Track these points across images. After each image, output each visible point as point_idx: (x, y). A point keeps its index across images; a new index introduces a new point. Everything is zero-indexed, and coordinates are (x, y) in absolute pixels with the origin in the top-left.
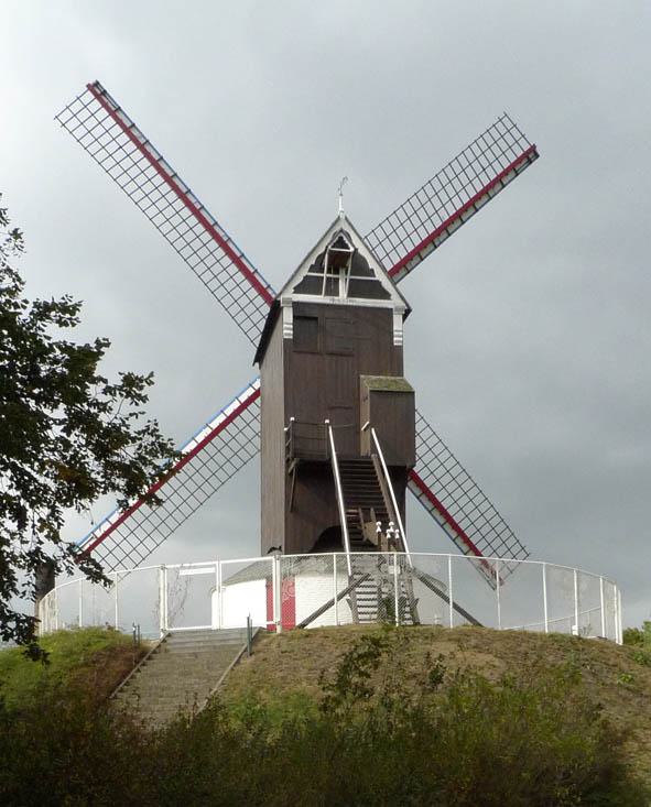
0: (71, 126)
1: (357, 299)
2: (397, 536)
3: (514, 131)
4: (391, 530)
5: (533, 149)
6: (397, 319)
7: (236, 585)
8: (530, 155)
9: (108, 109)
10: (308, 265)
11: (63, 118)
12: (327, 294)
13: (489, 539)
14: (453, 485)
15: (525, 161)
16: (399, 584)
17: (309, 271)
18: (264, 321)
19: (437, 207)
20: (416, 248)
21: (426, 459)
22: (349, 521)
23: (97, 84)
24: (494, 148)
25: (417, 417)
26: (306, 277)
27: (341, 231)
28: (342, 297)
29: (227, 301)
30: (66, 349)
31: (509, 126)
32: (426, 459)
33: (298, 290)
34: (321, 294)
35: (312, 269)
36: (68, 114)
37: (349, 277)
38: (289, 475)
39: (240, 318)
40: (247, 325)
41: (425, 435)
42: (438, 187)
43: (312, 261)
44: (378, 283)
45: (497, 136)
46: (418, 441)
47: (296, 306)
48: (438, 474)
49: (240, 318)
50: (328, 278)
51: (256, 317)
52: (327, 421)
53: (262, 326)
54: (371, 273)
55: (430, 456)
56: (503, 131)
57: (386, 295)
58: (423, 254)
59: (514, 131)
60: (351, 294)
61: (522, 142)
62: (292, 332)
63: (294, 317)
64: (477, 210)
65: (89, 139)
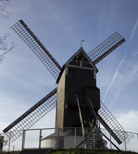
0: (15, 29)
3: (119, 35)
5: (124, 39)
6: (95, 72)
7: (49, 135)
9: (27, 29)
11: (13, 27)
13: (110, 121)
15: (122, 41)
16: (93, 141)
17: (73, 60)
18: (59, 74)
19: (93, 55)
20: (103, 54)
23: (22, 20)
24: (101, 49)
26: (71, 61)
27: (82, 51)
28: (81, 67)
33: (69, 64)
35: (73, 59)
36: (14, 27)
37: (83, 62)
38: (65, 109)
40: (55, 75)
43: (74, 57)
44: (90, 64)
45: (105, 44)
47: (69, 67)
50: (76, 62)
51: (57, 73)
53: (58, 75)
54: (89, 62)
56: (103, 45)
57: (92, 67)
58: (105, 55)
59: (119, 35)
60: (83, 66)
61: (121, 37)
63: (68, 70)
64: (108, 54)
65: (19, 32)
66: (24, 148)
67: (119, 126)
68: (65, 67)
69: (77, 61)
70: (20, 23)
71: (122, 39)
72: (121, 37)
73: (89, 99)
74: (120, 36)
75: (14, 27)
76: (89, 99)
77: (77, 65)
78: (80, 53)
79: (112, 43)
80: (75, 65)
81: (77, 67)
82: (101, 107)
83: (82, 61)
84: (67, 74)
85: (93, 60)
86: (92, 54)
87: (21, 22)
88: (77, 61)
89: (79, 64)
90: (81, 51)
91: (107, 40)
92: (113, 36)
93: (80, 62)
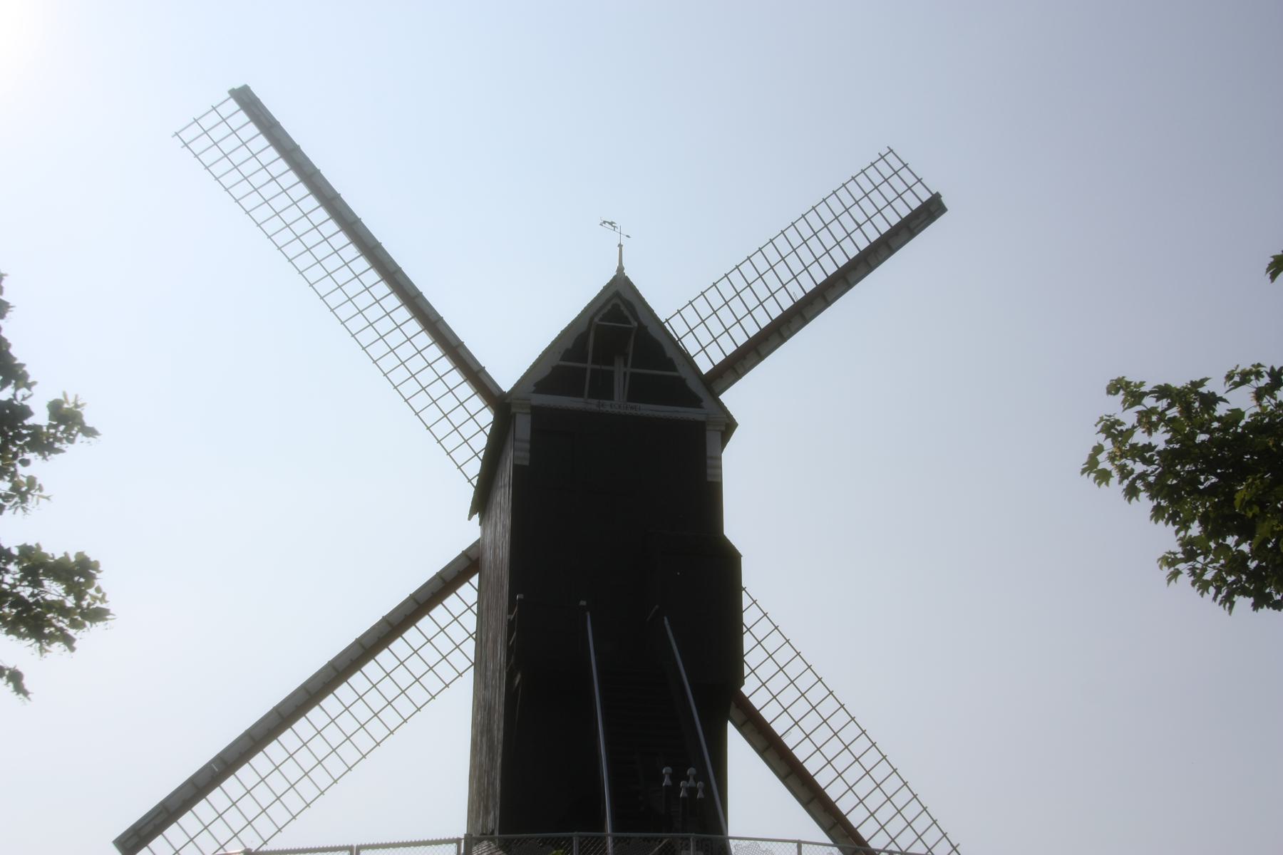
1: (643, 406)
2: (700, 795)
3: (904, 173)
4: (691, 783)
8: (932, 209)
10: (600, 315)
12: (592, 395)
14: (791, 694)
17: (600, 321)
21: (764, 672)
22: (630, 838)
25: (746, 601)
28: (618, 404)
29: (431, 415)
30: (1113, 464)
31: (897, 165)
32: (764, 672)
34: (612, 373)
36: (196, 130)
39: (450, 443)
41: (761, 630)
42: (751, 275)
46: (748, 641)
48: (786, 698)
49: (450, 443)
52: (583, 603)
55: (770, 668)
59: (904, 173)
61: (918, 189)
62: (528, 455)
66: (678, 337)
67: (863, 743)
68: (513, 410)
69: (589, 366)
70: (233, 105)
71: (926, 196)
72: (918, 189)
73: (666, 622)
74: (911, 180)
75: (196, 130)
76: (666, 622)
77: (591, 396)
78: (605, 311)
79: (859, 226)
80: (579, 394)
81: (592, 405)
82: (745, 629)
83: (626, 364)
84: (526, 463)
85: (705, 366)
86: (705, 311)
87: (246, 100)
88: (589, 366)
89: (603, 388)
90: (614, 301)
91: (822, 209)
92: (871, 172)
93: (611, 373)
